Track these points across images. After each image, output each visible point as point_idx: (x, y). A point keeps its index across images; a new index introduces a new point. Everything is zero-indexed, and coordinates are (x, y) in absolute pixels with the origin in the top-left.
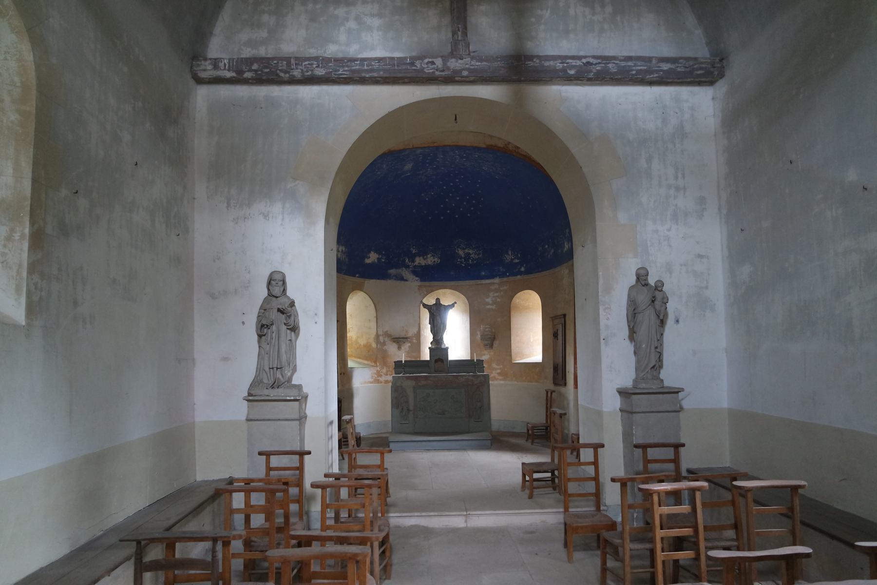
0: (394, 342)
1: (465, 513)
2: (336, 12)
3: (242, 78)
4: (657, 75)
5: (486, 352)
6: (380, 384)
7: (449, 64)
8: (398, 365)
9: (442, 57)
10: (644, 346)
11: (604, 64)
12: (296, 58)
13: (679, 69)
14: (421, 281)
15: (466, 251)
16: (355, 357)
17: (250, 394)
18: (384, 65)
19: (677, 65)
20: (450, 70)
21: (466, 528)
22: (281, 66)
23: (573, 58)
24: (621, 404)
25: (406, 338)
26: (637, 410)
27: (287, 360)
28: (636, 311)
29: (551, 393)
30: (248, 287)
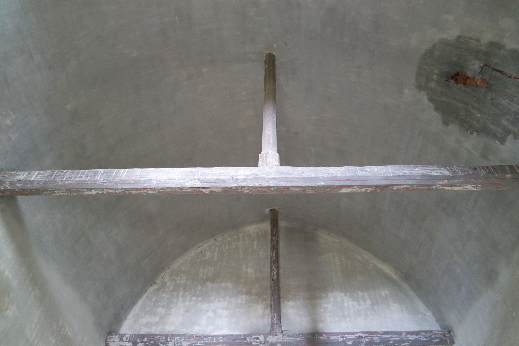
2: (202, 307)
4: (408, 343)
7: (268, 339)
9: (264, 334)
12: (172, 335)
13: (422, 339)
18: (227, 340)
19: (420, 336)
20: (269, 343)
22: (162, 340)
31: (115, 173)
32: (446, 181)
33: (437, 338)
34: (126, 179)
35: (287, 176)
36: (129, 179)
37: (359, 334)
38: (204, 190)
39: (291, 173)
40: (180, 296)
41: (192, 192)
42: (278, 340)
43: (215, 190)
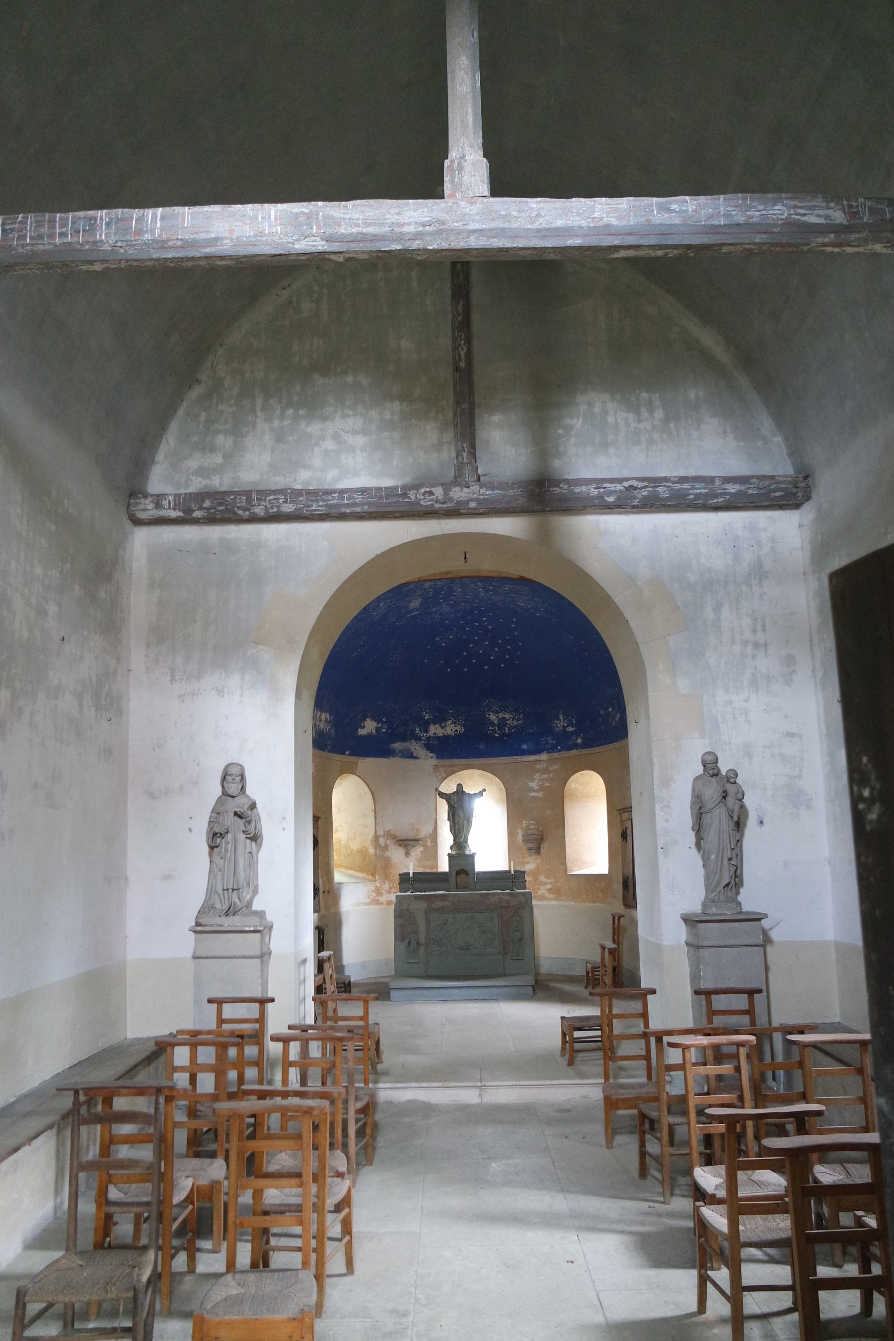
0: (400, 845)
1: (479, 1084)
2: (309, 429)
3: (190, 518)
4: (722, 499)
5: (530, 859)
6: (378, 906)
7: (451, 494)
8: (405, 880)
9: (442, 485)
10: (713, 857)
11: (651, 487)
12: (259, 492)
13: (750, 492)
14: (438, 758)
15: (501, 715)
16: (345, 867)
17: (198, 924)
18: (369, 498)
19: (747, 486)
21: (480, 1106)
22: (240, 502)
23: (612, 481)
24: (687, 936)
25: (418, 840)
26: (706, 943)
27: (246, 880)
28: (702, 811)
29: (619, 919)
30: (196, 783)
31: (134, 220)
32: (832, 236)
33: (780, 490)
34: (164, 237)
35: (506, 225)
36: (171, 238)
37: (630, 481)
38: (333, 257)
39: (515, 217)
40: (258, 408)
41: (308, 260)
42: (471, 495)
43: (356, 256)
